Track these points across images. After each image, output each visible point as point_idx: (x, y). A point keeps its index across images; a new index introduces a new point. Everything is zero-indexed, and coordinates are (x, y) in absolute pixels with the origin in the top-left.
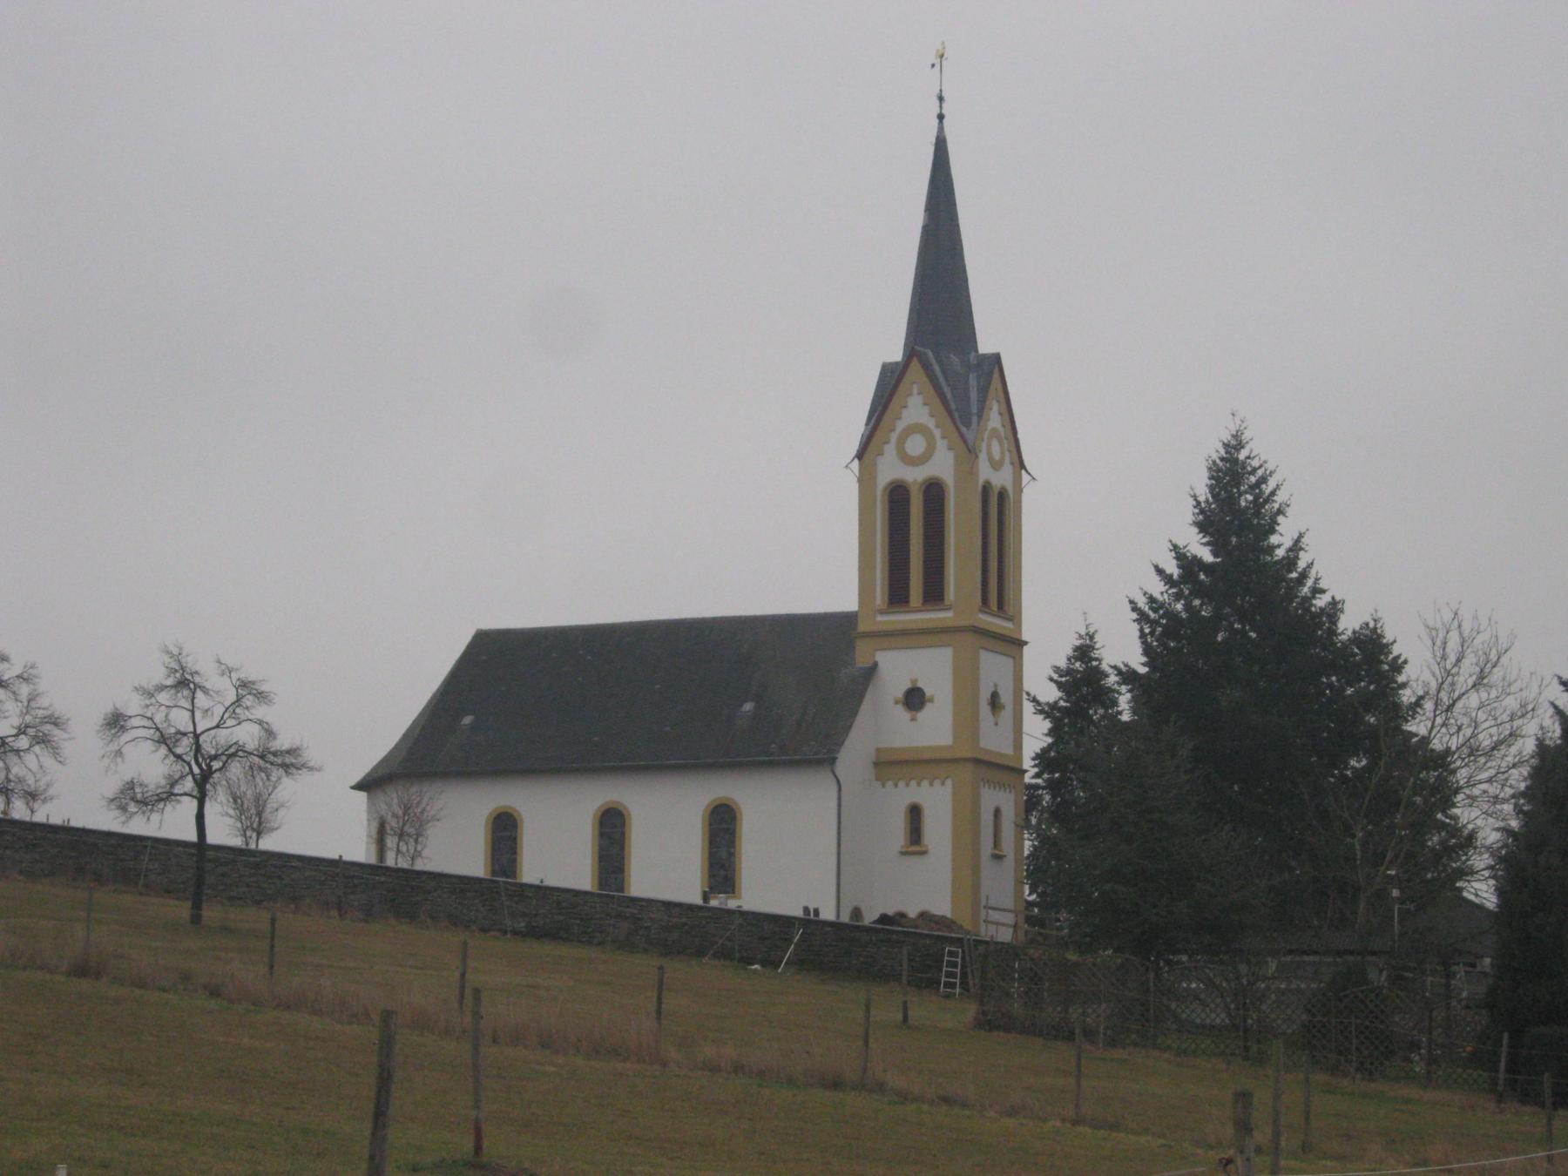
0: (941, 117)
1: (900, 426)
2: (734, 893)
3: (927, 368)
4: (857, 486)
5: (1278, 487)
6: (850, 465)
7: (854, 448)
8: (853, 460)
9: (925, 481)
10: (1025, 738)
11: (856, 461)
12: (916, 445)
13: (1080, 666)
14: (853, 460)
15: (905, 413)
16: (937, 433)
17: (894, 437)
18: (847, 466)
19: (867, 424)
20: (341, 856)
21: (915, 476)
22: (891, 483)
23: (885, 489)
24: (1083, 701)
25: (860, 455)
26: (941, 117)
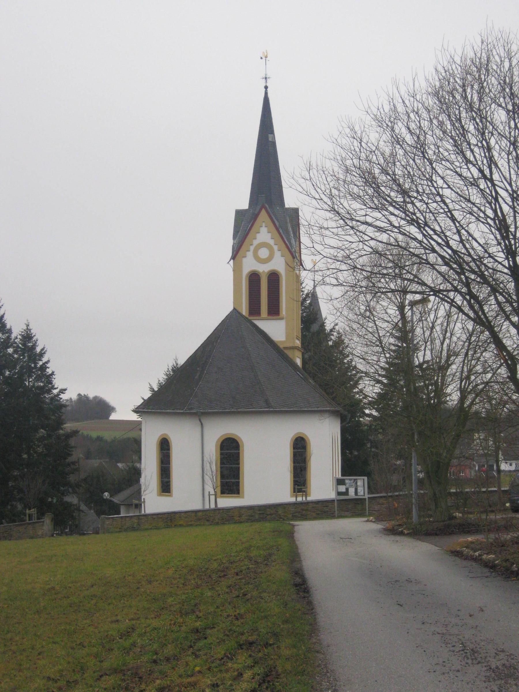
0: (266, 87)
1: (256, 243)
2: (238, 493)
3: (267, 211)
4: (232, 273)
5: (301, 525)
6: (230, 262)
7: (230, 254)
8: (230, 260)
9: (268, 273)
10: (302, 255)
11: (232, 261)
12: (264, 253)
13: (142, 672)
14: (230, 260)
15: (258, 236)
16: (276, 248)
17: (252, 248)
18: (228, 263)
19: (234, 237)
20: (87, 394)
21: (264, 269)
22: (249, 273)
23: (248, 274)
24: (406, 494)
25: (234, 257)
26: (266, 87)
